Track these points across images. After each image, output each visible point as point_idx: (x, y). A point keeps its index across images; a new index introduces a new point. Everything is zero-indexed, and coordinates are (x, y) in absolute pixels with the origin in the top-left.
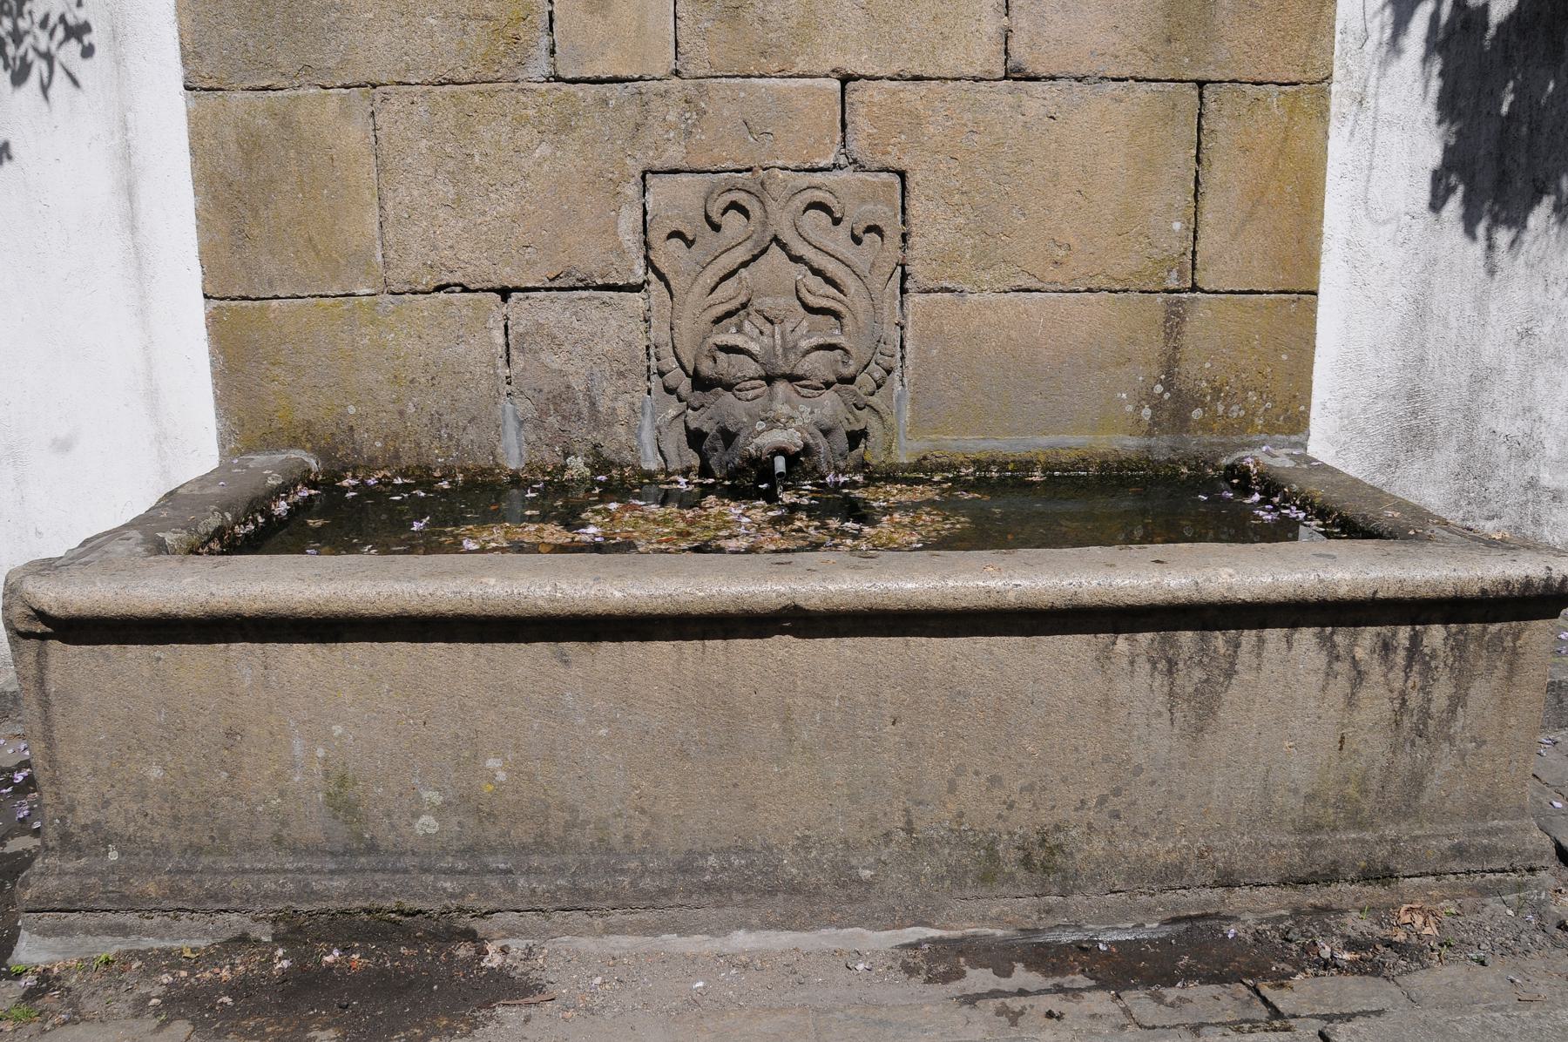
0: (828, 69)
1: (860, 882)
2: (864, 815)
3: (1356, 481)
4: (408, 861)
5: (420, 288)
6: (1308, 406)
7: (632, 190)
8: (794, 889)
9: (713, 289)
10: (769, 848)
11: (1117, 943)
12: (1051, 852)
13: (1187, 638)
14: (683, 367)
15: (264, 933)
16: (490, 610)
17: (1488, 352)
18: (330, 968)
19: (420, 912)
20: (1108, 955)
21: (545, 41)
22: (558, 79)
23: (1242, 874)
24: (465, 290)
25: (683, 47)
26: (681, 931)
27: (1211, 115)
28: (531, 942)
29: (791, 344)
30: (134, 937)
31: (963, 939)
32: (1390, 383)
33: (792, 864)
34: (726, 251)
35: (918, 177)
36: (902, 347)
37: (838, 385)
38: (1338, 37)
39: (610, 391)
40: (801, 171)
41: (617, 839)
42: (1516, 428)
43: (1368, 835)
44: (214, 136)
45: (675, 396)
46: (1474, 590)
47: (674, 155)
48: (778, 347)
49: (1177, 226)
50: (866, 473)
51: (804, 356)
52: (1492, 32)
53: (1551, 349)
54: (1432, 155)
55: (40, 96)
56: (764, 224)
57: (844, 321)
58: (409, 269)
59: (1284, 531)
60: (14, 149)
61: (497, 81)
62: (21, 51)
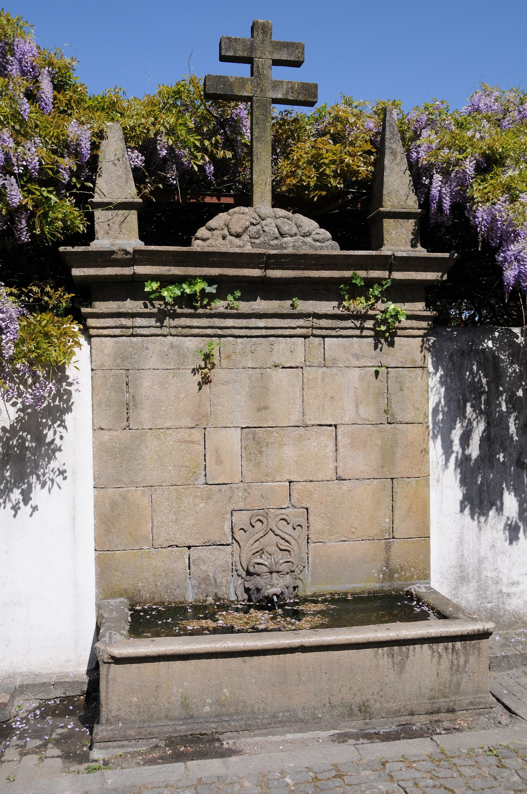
0: (285, 479)
1: (318, 718)
2: (318, 699)
3: (443, 597)
4: (202, 720)
5: (164, 546)
6: (430, 571)
7: (228, 516)
8: (302, 721)
10: (295, 710)
11: (385, 732)
12: (366, 707)
13: (396, 648)
14: (243, 568)
15: (162, 744)
16: (229, 650)
17: (482, 553)
18: (183, 752)
19: (206, 734)
20: (383, 735)
21: (203, 473)
22: (207, 484)
23: (416, 711)
24: (177, 546)
25: (244, 474)
26: (273, 734)
27: (395, 488)
28: (234, 741)
30: (126, 748)
31: (345, 733)
32: (454, 563)
33: (301, 714)
35: (312, 510)
36: (308, 559)
38: (431, 463)
39: (221, 576)
41: (256, 710)
42: (493, 575)
43: (447, 700)
44: (102, 502)
46: (466, 633)
47: (241, 506)
49: (387, 520)
52: (473, 462)
53: (501, 551)
54: (460, 497)
55: (48, 492)
56: (268, 525)
58: (160, 541)
59: (423, 616)
60: (39, 508)
61: (189, 485)
62: (44, 479)
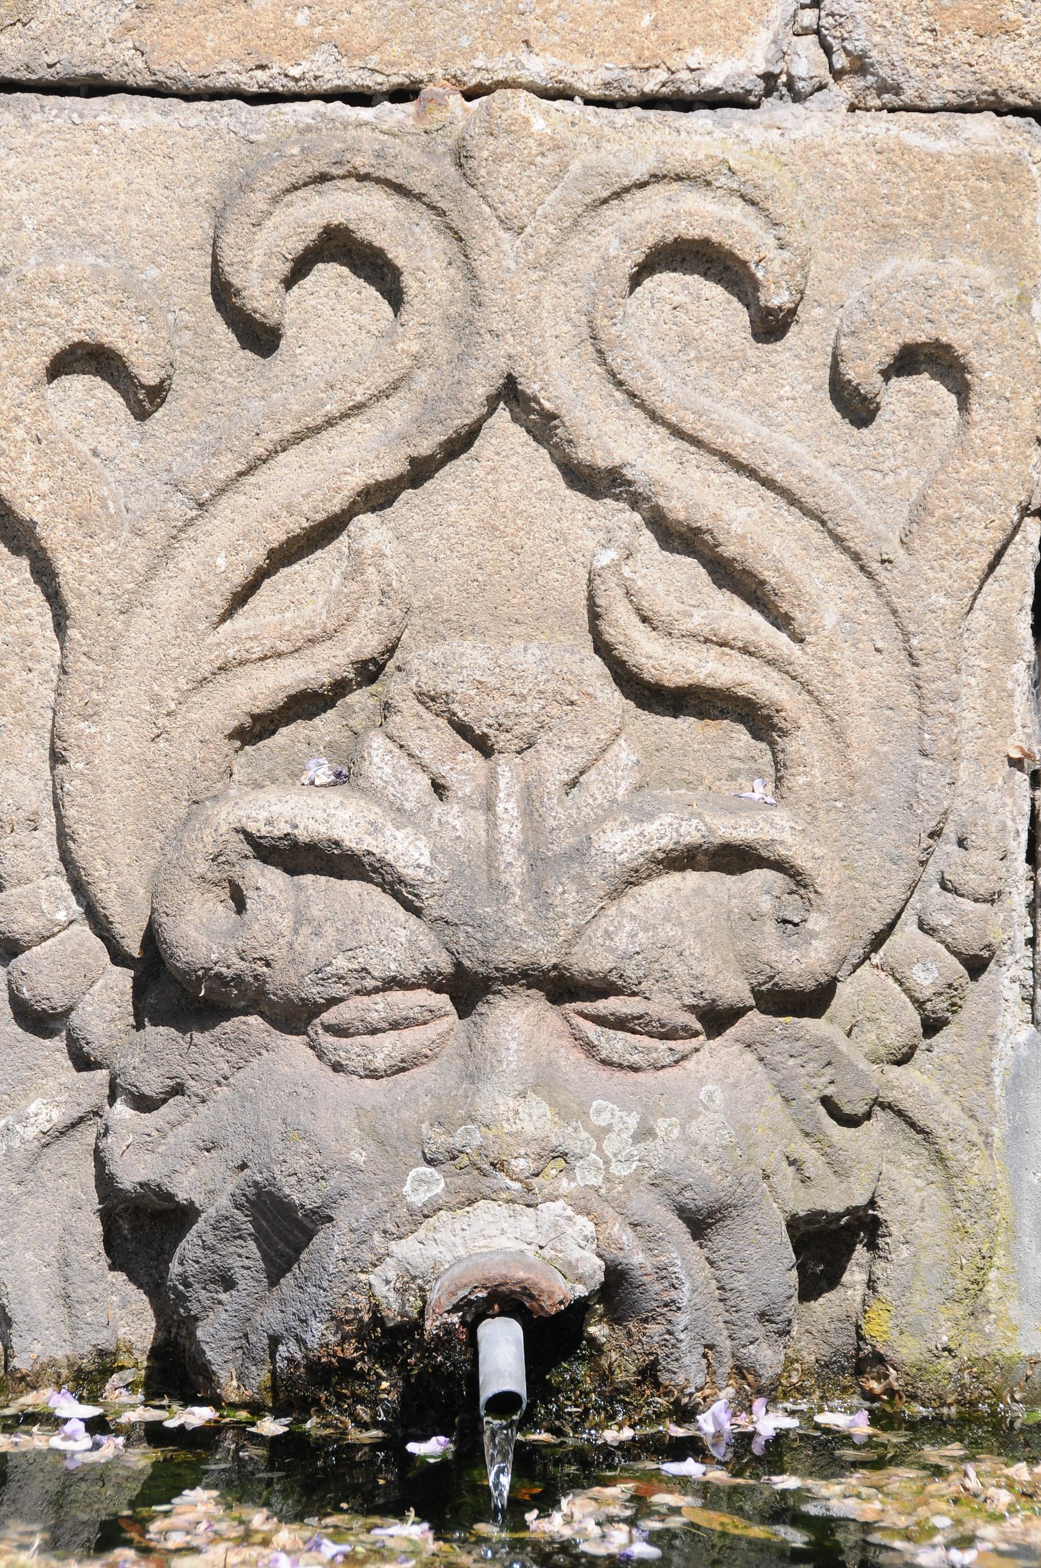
9: (241, 597)
29: (566, 841)
34: (298, 438)
37: (755, 1019)
40: (628, 103)
45: (58, 1043)
48: (509, 853)
50: (870, 1396)
51: (615, 894)
57: (792, 746)
